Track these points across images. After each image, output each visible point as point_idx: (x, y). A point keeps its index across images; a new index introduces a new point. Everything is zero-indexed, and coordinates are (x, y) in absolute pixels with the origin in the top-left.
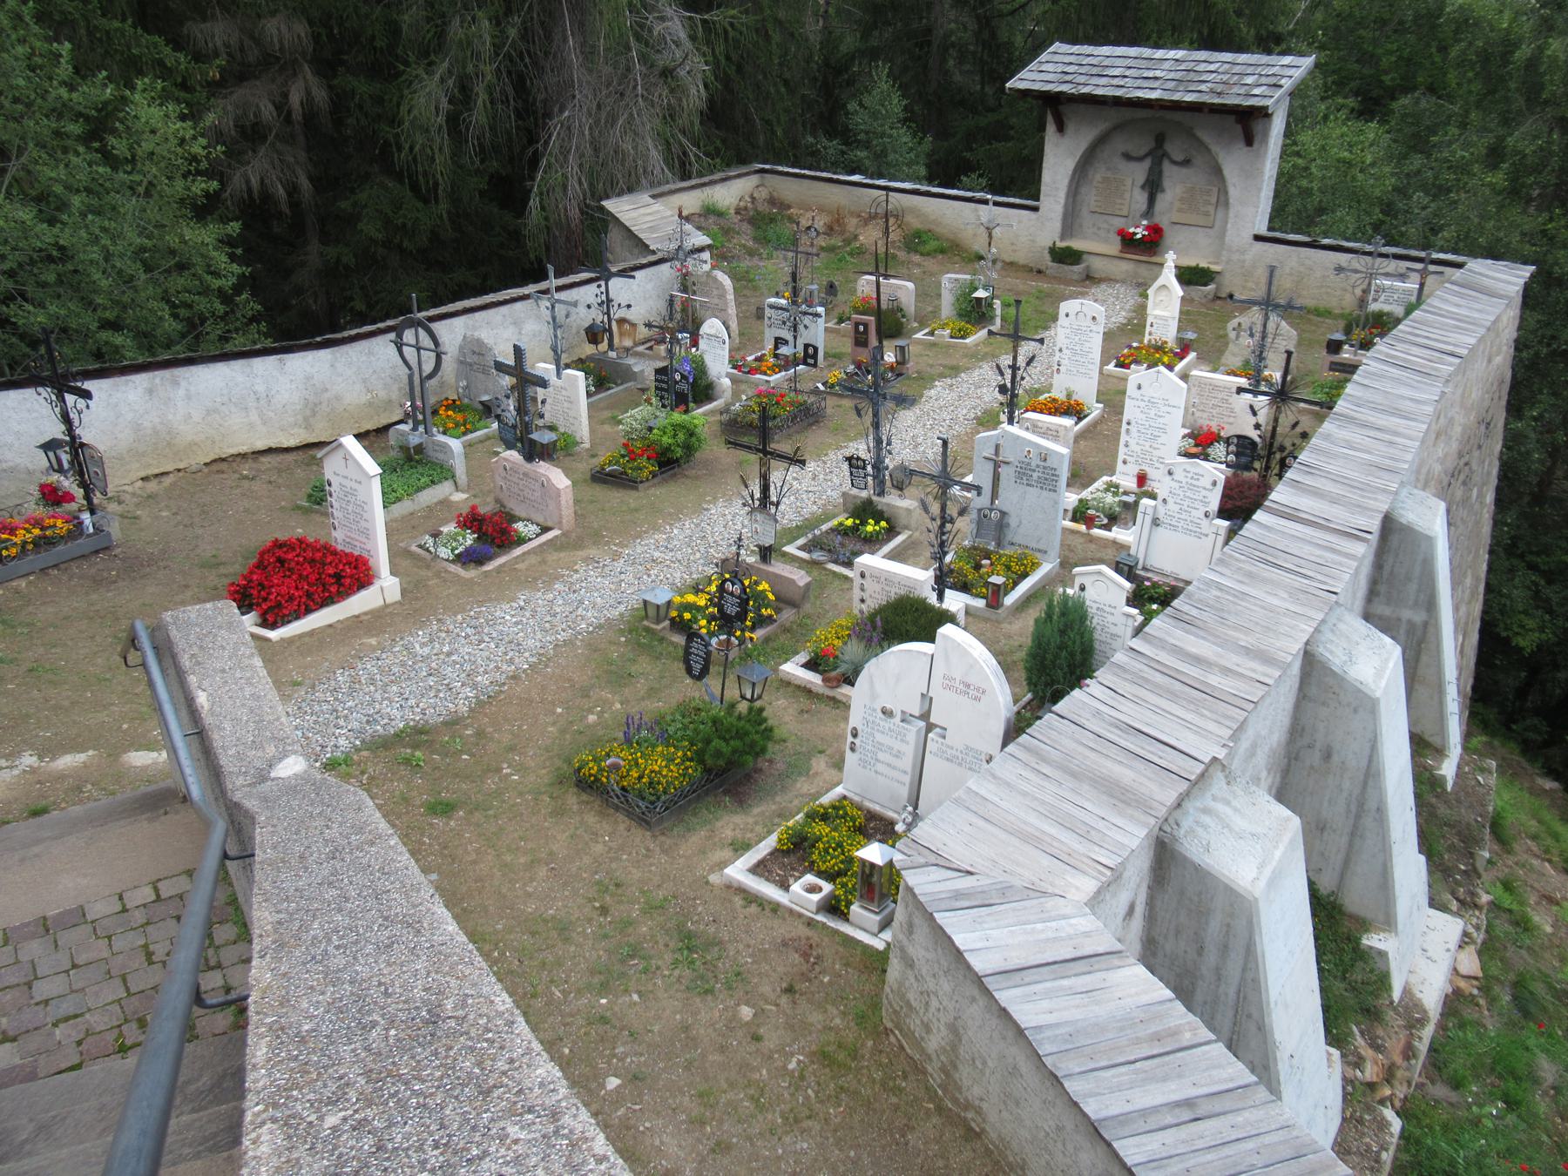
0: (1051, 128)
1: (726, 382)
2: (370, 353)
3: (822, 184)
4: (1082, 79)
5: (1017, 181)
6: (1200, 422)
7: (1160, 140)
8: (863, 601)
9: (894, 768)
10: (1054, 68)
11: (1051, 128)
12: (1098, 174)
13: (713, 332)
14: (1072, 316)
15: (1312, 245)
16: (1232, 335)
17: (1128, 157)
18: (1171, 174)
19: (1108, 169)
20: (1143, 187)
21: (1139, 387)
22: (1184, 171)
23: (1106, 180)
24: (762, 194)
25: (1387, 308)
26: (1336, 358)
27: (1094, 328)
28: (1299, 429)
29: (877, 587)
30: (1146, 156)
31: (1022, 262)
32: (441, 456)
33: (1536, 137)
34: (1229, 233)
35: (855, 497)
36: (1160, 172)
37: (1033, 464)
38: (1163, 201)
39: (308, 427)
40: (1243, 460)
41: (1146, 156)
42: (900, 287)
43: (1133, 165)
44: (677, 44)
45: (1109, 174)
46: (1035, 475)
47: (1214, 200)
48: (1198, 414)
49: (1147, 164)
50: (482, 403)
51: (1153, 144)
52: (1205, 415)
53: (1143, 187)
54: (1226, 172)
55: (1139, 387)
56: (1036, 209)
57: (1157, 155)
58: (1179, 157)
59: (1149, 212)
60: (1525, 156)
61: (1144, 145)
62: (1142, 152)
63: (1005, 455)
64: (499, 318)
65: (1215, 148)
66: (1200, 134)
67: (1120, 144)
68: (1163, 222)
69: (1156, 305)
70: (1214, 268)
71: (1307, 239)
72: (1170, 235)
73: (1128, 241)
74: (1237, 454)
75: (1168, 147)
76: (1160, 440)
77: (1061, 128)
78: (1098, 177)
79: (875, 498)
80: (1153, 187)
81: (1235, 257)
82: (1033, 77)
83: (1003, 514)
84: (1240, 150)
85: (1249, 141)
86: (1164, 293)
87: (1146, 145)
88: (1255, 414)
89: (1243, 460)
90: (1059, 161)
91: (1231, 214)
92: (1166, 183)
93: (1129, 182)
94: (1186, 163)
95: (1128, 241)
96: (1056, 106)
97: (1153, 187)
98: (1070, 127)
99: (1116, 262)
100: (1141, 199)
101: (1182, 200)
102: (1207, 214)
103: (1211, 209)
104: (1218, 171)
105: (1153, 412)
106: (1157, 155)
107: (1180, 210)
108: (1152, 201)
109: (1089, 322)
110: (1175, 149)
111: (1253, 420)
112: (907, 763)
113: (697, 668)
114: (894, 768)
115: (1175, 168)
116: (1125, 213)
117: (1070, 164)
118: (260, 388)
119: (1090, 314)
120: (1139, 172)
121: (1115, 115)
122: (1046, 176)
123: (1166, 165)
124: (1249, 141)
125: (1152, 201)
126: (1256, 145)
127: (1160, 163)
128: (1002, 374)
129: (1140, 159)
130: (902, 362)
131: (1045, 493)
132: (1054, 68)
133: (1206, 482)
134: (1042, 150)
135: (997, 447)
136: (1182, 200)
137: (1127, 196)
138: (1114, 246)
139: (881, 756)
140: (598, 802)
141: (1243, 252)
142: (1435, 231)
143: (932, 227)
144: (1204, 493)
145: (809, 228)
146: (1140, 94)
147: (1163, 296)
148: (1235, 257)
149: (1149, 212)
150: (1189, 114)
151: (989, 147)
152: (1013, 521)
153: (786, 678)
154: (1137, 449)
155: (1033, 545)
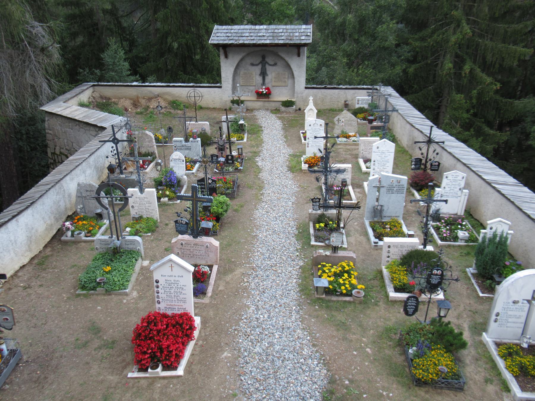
0: (222, 57)
1: (185, 177)
2: (44, 204)
3: (123, 88)
4: (237, 38)
5: (214, 78)
6: (365, 155)
7: (264, 57)
8: (388, 257)
9: (517, 323)
10: (220, 34)
11: (222, 57)
12: (242, 72)
13: (177, 157)
14: (312, 126)
16: (336, 123)
17: (252, 65)
18: (269, 69)
19: (245, 70)
20: (260, 75)
21: (378, 148)
22: (274, 67)
24: (97, 95)
25: (362, 106)
26: (372, 125)
27: (321, 128)
28: (436, 152)
29: (396, 250)
32: (131, 246)
33: (349, 46)
34: (296, 88)
35: (315, 214)
38: (268, 79)
39: (30, 250)
40: (417, 166)
42: (204, 124)
44: (44, 37)
45: (246, 71)
46: (395, 189)
47: (287, 77)
48: (364, 153)
49: (260, 67)
50: (97, 214)
52: (367, 153)
53: (260, 75)
54: (292, 66)
55: (378, 148)
56: (220, 87)
57: (263, 63)
58: (272, 63)
61: (258, 60)
62: (257, 62)
63: (384, 184)
64: (79, 171)
65: (287, 59)
66: (280, 54)
67: (249, 60)
69: (308, 116)
70: (293, 100)
71: (323, 86)
72: (274, 91)
73: (260, 95)
74: (415, 165)
76: (387, 165)
77: (226, 57)
78: (242, 73)
79: (325, 213)
80: (264, 74)
81: (300, 95)
83: (382, 206)
84: (296, 58)
85: (299, 55)
86: (311, 111)
87: (259, 60)
88: (421, 149)
89: (417, 166)
90: (227, 69)
91: (296, 81)
92: (268, 72)
93: (254, 73)
94: (275, 64)
95: (260, 95)
97: (264, 74)
98: (230, 56)
100: (259, 79)
101: (275, 78)
102: (285, 82)
106: (263, 63)
107: (275, 82)
108: (264, 79)
111: (420, 152)
112: (523, 320)
113: (411, 311)
114: (517, 323)
115: (271, 67)
116: (254, 84)
117: (232, 69)
118: (12, 238)
119: (319, 124)
120: (257, 70)
122: (223, 75)
123: (267, 66)
124: (299, 55)
125: (264, 79)
126: (301, 56)
127: (265, 66)
128: (321, 152)
129: (257, 65)
130: (240, 155)
131: (399, 195)
132: (220, 34)
133: (460, 178)
136: (275, 78)
137: (254, 78)
138: (254, 98)
139: (510, 320)
140: (431, 389)
142: (333, 77)
143: (178, 99)
144: (459, 182)
145: (157, 107)
146: (263, 42)
147: (311, 112)
148: (300, 95)
149: (263, 84)
150: (276, 48)
152: (385, 208)
153: (394, 299)
154: (378, 170)
155: (394, 215)
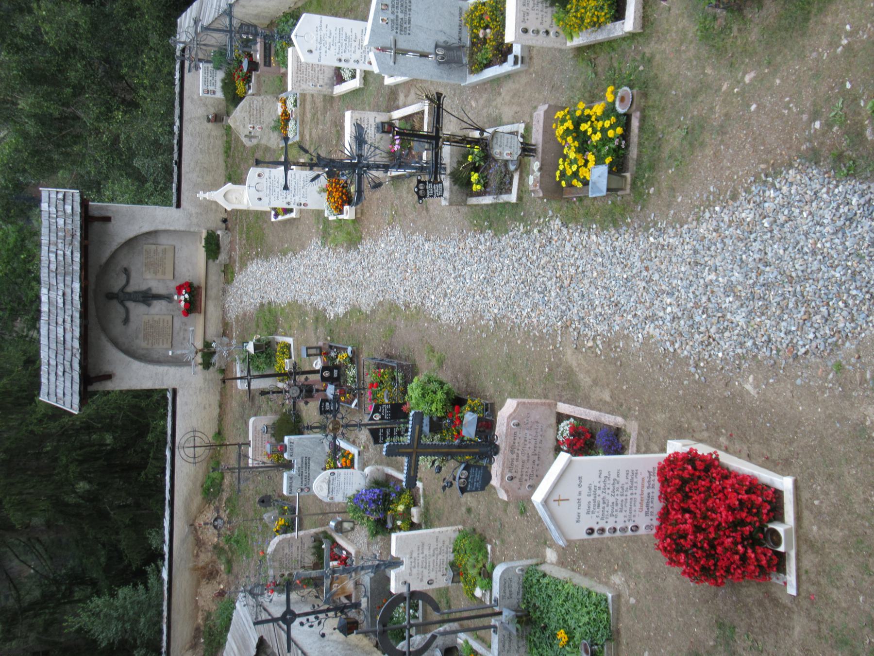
0: (109, 386)
3: (174, 600)
5: (154, 405)
7: (111, 296)
8: (547, 32)
11: (109, 386)
12: (141, 344)
13: (325, 486)
14: (260, 195)
15: (179, 164)
16: (255, 141)
17: (126, 321)
19: (137, 338)
20: (149, 305)
21: (310, 51)
22: (133, 274)
23: (146, 337)
25: (219, 84)
26: (261, 64)
27: (267, 175)
29: (532, 15)
30: (124, 306)
31: (218, 398)
34: (177, 228)
35: (451, 191)
36: (135, 292)
37: (392, 17)
38: (158, 288)
41: (124, 306)
43: (132, 317)
45: (141, 336)
46: (401, 16)
47: (154, 247)
48: (321, 82)
49: (131, 305)
51: (115, 302)
52: (321, 77)
53: (149, 305)
55: (310, 51)
56: (175, 392)
57: (123, 297)
58: (123, 278)
59: (168, 298)
60: (100, 112)
61: (116, 310)
62: (122, 310)
63: (388, 41)
65: (114, 246)
67: (117, 328)
68: (174, 285)
69: (240, 202)
73: (192, 307)
75: (116, 289)
76: (349, 33)
77: (109, 377)
78: (144, 344)
79: (448, 171)
80: (147, 297)
81: (194, 220)
82: (71, 404)
83: (437, 46)
84: (114, 226)
85: (108, 219)
86: (229, 196)
87: (115, 305)
90: (134, 376)
91: (163, 227)
92: (144, 287)
94: (127, 271)
95: (192, 307)
96: (90, 378)
97: (147, 297)
98: (107, 369)
99: (209, 315)
100: (159, 306)
101: (155, 273)
102: (165, 251)
103: (160, 248)
104: (131, 243)
105: (329, 40)
106: (123, 297)
107: (164, 273)
109: (263, 180)
110: (117, 283)
115: (132, 282)
117: (136, 365)
120: (137, 310)
121: (94, 331)
122: (147, 385)
123: (131, 289)
124: (108, 219)
126: (109, 214)
127: (129, 294)
128: (318, 176)
129: (127, 311)
134: (128, 391)
135: (383, 49)
136: (155, 273)
137: (156, 318)
138: (198, 319)
141: (191, 215)
143: (199, 484)
146: (77, 297)
149: (168, 298)
151: (126, 440)
152: (442, 39)
153: (639, 22)
154: (358, 52)
